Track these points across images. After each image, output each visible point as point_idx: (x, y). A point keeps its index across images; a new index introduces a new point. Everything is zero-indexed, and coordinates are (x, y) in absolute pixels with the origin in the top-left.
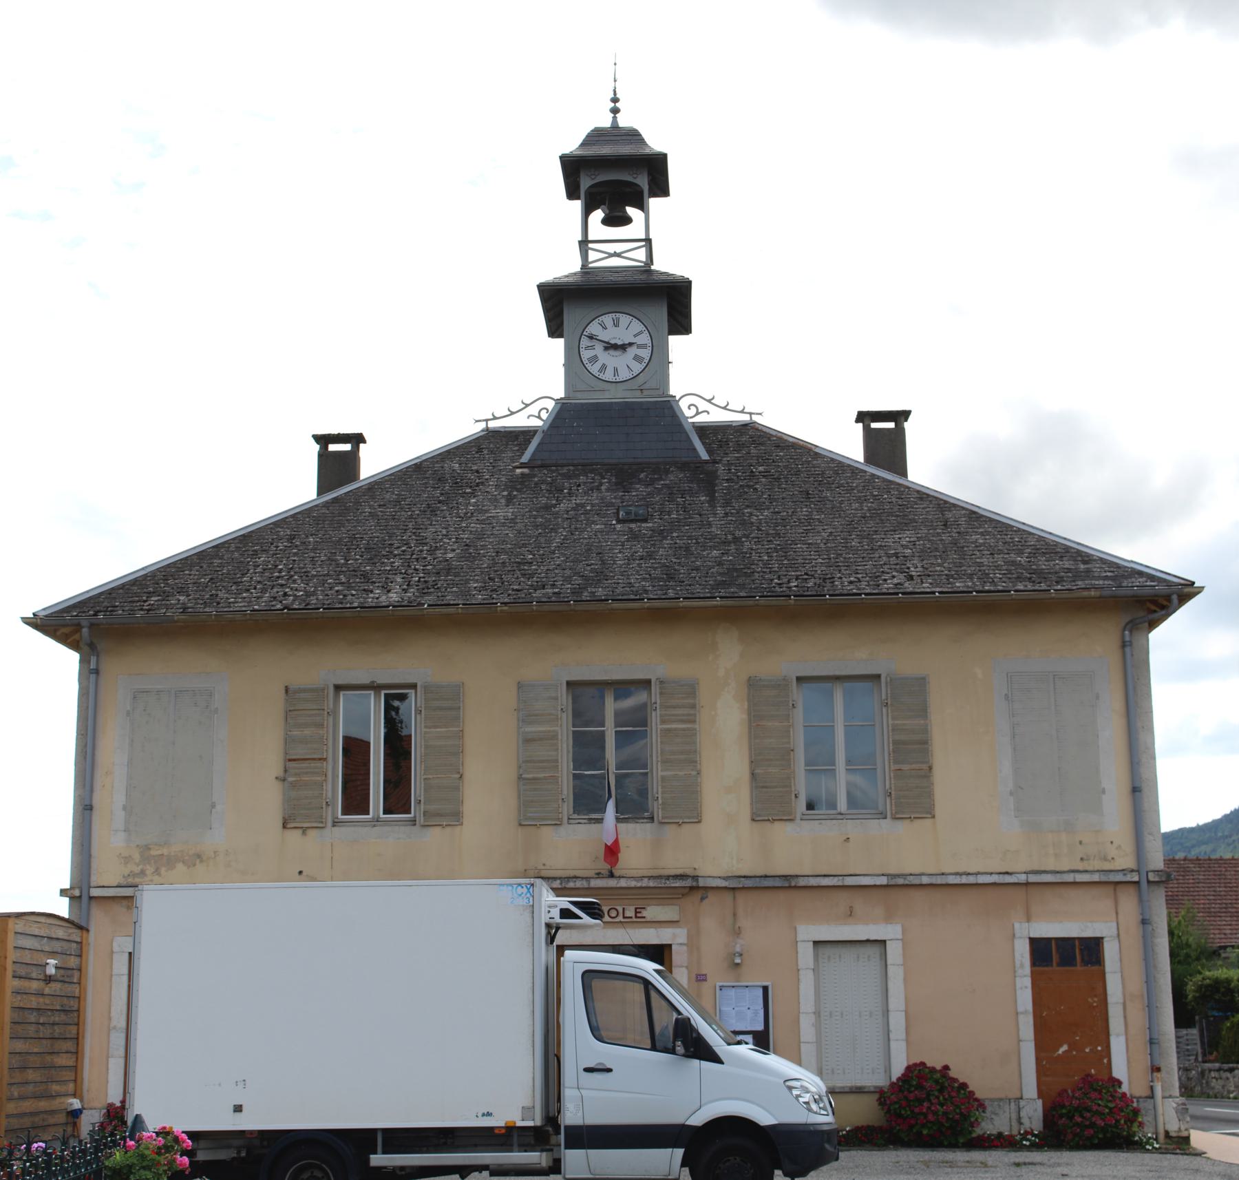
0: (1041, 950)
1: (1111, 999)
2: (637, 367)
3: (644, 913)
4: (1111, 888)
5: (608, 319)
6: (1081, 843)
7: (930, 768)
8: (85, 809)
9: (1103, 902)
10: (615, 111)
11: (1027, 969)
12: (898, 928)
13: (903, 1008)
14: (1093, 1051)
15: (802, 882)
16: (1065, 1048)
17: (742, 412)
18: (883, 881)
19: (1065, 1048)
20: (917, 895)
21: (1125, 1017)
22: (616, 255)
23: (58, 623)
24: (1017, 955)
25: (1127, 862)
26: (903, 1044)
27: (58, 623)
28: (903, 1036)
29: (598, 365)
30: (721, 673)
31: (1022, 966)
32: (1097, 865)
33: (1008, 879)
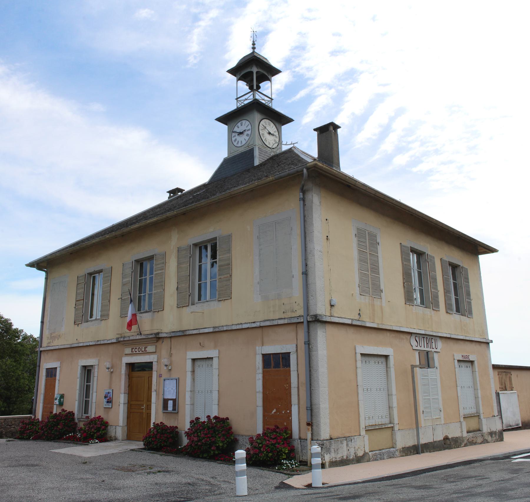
0: (267, 359)
1: (187, 385)
2: (247, 138)
3: (147, 349)
4: (294, 326)
5: (239, 124)
6: (283, 304)
7: (231, 276)
8: (42, 322)
9: (289, 334)
10: (254, 48)
11: (260, 370)
12: (217, 351)
13: (217, 389)
14: (286, 412)
15: (188, 333)
16: (274, 411)
17: (291, 144)
18: (211, 330)
19: (274, 411)
20: (224, 335)
21: (299, 395)
22: (246, 99)
23: (38, 265)
24: (257, 363)
25: (300, 312)
26: (217, 406)
27: (38, 265)
28: (217, 403)
29: (237, 142)
30: (172, 248)
31: (259, 368)
32: (290, 315)
33: (254, 325)
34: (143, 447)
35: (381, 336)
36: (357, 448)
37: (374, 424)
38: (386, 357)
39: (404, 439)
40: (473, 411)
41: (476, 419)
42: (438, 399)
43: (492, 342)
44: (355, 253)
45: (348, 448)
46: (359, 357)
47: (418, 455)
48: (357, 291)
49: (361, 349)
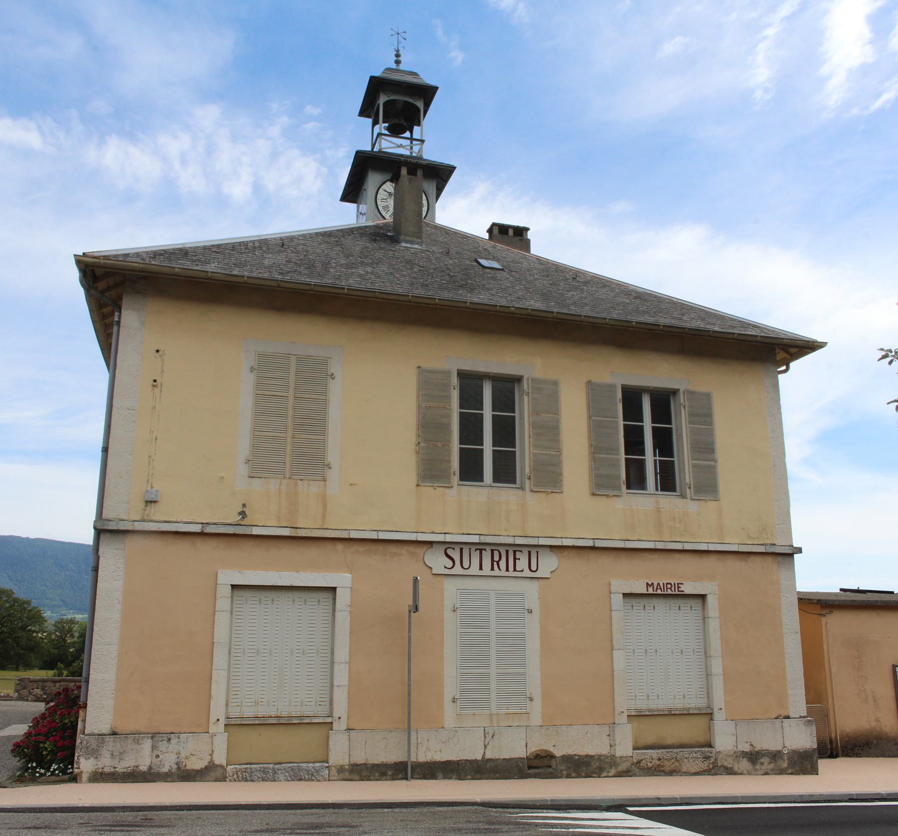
13: (614, 652)
28: (337, 667)
34: (804, 713)
35: (312, 552)
36: (183, 755)
37: (266, 714)
38: (703, 597)
39: (340, 751)
40: (701, 703)
41: (702, 722)
42: (488, 675)
43: (799, 550)
44: (245, 401)
45: (156, 752)
46: (617, 600)
47: (404, 782)
48: (243, 470)
49: (229, 577)
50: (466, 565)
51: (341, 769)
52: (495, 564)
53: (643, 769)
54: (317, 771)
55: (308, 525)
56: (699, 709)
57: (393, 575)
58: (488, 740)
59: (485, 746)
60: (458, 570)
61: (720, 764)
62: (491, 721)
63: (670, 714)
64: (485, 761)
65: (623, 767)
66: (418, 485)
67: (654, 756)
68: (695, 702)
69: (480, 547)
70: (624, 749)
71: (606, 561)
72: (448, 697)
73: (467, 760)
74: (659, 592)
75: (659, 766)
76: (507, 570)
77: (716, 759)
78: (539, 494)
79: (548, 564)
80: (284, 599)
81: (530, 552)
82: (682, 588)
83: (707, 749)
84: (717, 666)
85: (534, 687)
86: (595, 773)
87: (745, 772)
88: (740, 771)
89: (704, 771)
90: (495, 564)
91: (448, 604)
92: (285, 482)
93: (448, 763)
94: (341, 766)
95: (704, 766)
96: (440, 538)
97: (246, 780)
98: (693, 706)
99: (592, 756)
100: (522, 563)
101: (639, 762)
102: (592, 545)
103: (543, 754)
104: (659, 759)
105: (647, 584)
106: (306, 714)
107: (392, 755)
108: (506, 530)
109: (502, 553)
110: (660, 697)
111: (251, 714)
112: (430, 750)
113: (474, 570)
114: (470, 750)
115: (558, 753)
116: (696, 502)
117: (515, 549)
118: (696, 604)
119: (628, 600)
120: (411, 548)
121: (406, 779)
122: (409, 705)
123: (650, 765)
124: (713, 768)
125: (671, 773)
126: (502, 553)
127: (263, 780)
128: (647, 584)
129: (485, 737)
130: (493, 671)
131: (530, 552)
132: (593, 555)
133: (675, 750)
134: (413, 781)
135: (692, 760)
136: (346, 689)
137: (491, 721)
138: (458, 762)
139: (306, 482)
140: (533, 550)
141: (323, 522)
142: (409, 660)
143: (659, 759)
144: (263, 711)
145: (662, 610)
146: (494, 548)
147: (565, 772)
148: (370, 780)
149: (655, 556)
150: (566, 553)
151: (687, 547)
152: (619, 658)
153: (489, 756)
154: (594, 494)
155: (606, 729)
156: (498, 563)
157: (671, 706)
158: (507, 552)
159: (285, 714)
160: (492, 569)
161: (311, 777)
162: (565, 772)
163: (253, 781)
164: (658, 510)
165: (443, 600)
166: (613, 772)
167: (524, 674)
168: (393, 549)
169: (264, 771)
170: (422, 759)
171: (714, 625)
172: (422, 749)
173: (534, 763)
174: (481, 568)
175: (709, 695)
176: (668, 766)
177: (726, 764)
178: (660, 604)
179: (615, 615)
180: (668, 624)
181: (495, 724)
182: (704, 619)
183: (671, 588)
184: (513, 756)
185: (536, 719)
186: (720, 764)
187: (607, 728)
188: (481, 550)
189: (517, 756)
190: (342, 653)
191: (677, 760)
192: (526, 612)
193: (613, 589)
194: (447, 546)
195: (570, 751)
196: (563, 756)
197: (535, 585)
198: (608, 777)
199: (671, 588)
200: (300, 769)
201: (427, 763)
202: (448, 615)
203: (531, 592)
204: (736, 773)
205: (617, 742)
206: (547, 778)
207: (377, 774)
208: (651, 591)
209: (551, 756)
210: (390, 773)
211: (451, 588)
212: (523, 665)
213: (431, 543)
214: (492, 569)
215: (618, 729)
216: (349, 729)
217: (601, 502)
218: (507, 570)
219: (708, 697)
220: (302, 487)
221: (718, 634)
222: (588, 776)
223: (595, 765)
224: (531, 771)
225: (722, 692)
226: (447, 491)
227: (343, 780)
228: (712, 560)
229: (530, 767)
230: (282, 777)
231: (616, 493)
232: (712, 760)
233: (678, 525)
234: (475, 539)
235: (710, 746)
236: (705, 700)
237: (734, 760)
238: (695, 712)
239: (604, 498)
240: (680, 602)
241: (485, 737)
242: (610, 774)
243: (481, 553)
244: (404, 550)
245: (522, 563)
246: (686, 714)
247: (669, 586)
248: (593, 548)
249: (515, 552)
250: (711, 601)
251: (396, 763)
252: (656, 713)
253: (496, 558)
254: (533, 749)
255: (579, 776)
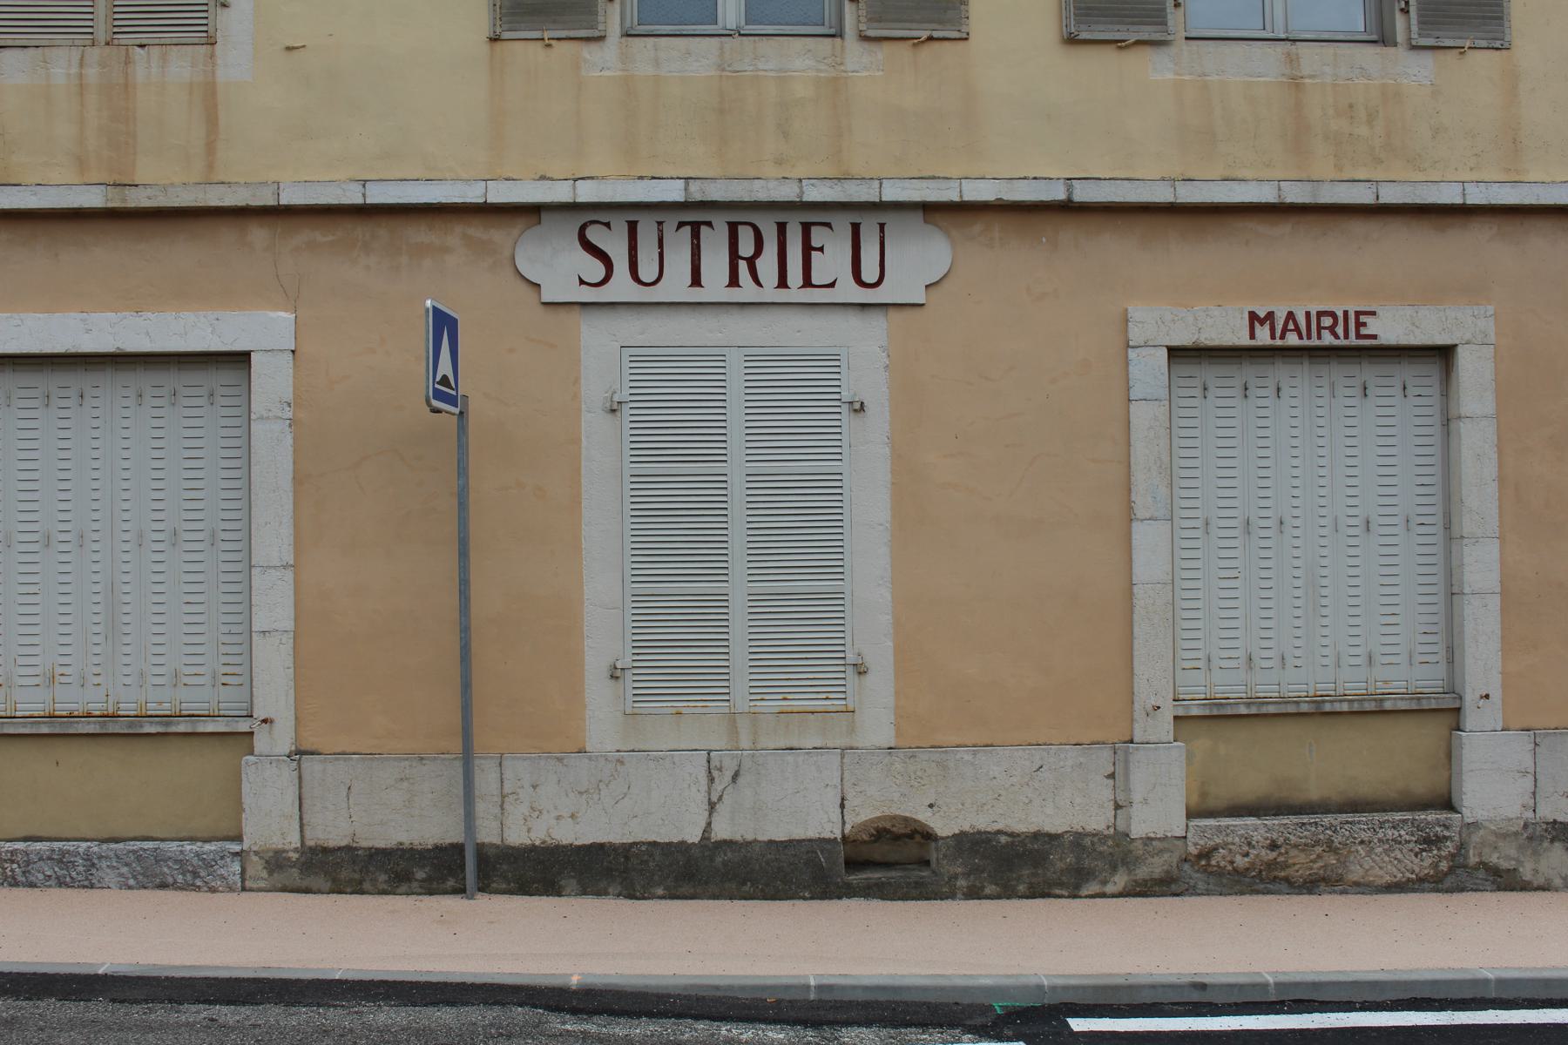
13: (1137, 527)
35: (179, 253)
37: (78, 708)
38: (1443, 355)
39: (270, 815)
40: (1425, 678)
41: (1427, 735)
42: (723, 598)
46: (1150, 368)
50: (647, 271)
51: (276, 862)
52: (743, 266)
53: (1220, 873)
54: (208, 865)
55: (164, 180)
56: (1417, 696)
57: (383, 300)
58: (718, 787)
59: (712, 806)
60: (621, 287)
61: (1473, 859)
62: (733, 730)
63: (1319, 713)
64: (710, 847)
65: (1154, 867)
66: (494, 39)
67: (1257, 837)
68: (1405, 674)
69: (693, 216)
70: (1159, 812)
71: (1114, 248)
72: (595, 664)
73: (655, 844)
74: (1292, 339)
75: (1271, 865)
76: (783, 283)
77: (1462, 846)
78: (886, 46)
79: (916, 261)
80: (110, 390)
81: (856, 229)
82: (1372, 326)
83: (1431, 816)
84: (1481, 567)
85: (871, 627)
86: (1061, 885)
87: (1558, 882)
88: (1540, 881)
89: (1421, 880)
90: (743, 266)
91: (594, 391)
92: (94, 54)
93: (597, 851)
94: (278, 852)
95: (1423, 864)
96: (560, 193)
97: (15, 883)
98: (1398, 686)
99: (1053, 837)
100: (832, 261)
101: (1206, 854)
102: (1061, 195)
103: (899, 829)
104: (1274, 846)
105: (1253, 316)
106: (188, 708)
107: (426, 824)
108: (779, 162)
109: (763, 233)
110: (1290, 662)
111: (37, 709)
112: (540, 809)
113: (676, 285)
114: (670, 814)
115: (944, 826)
116: (1428, 55)
117: (809, 217)
118: (1423, 377)
119: (1185, 369)
120: (475, 230)
121: (460, 891)
122: (471, 687)
123: (1241, 862)
124: (1451, 870)
125: (1311, 885)
126: (763, 233)
127: (61, 883)
128: (1253, 316)
129: (712, 780)
130: (739, 588)
131: (856, 229)
132: (1068, 231)
133: (1327, 819)
134: (487, 904)
135: (1381, 848)
136: (288, 640)
137: (733, 730)
138: (626, 850)
139: (155, 51)
140: (867, 217)
141: (210, 167)
142: (464, 554)
143: (1274, 846)
144: (70, 699)
145: (1301, 406)
146: (739, 216)
147: (962, 883)
148: (362, 892)
149: (1283, 228)
150: (977, 228)
151: (1390, 195)
152: (1149, 541)
153: (721, 831)
154: (1072, 41)
155: (1103, 760)
156: (751, 262)
157: (1325, 688)
158: (782, 228)
159: (128, 708)
160: (734, 281)
161: (195, 878)
162: (962, 883)
163: (32, 885)
164: (1296, 83)
165: (577, 381)
166: (1120, 880)
167: (838, 596)
168: (419, 233)
169: (62, 860)
170: (517, 836)
171: (1477, 441)
172: (516, 812)
173: (881, 851)
174: (696, 281)
175: (1452, 655)
176: (1301, 864)
177: (1494, 859)
178: (1299, 381)
179: (1142, 415)
180: (1323, 450)
181: (745, 742)
182: (1447, 422)
183: (1332, 329)
184: (799, 833)
185: (877, 727)
186: (1473, 859)
187: (1105, 754)
188: (696, 228)
189: (812, 833)
190: (274, 538)
191: (1330, 847)
192: (845, 409)
193: (1136, 335)
194: (585, 218)
195: (983, 822)
196: (960, 837)
197: (874, 329)
198: (1103, 895)
199: (1332, 329)
200: (159, 858)
201: (533, 848)
202: (594, 424)
203: (863, 351)
204: (1525, 887)
205: (1137, 797)
206: (905, 897)
207: (383, 877)
208: (1263, 337)
209: (928, 836)
210: (420, 875)
211: (602, 346)
212: (836, 571)
213: (533, 212)
214: (734, 281)
215: (1139, 756)
216: (300, 753)
217: (1098, 65)
218: (783, 283)
219: (1451, 661)
220: (145, 66)
221: (1490, 469)
222: (1038, 892)
223: (1061, 861)
224: (856, 878)
225: (1495, 644)
226: (589, 52)
227: (284, 889)
228: (1478, 238)
229: (853, 864)
230: (110, 877)
231: (1146, 33)
232: (1450, 847)
233: (1363, 131)
234: (672, 192)
235: (1448, 805)
236: (1441, 671)
237: (1520, 848)
238: (1402, 705)
239: (1109, 53)
240: (1368, 372)
241: (712, 780)
242: (1109, 889)
243: (696, 236)
244: (454, 235)
245: (832, 261)
246: (1372, 712)
247: (1327, 321)
248: (1068, 208)
249: (806, 228)
250: (1472, 367)
251: (438, 849)
252: (1272, 709)
253: (746, 249)
254: (864, 812)
255: (1008, 893)
